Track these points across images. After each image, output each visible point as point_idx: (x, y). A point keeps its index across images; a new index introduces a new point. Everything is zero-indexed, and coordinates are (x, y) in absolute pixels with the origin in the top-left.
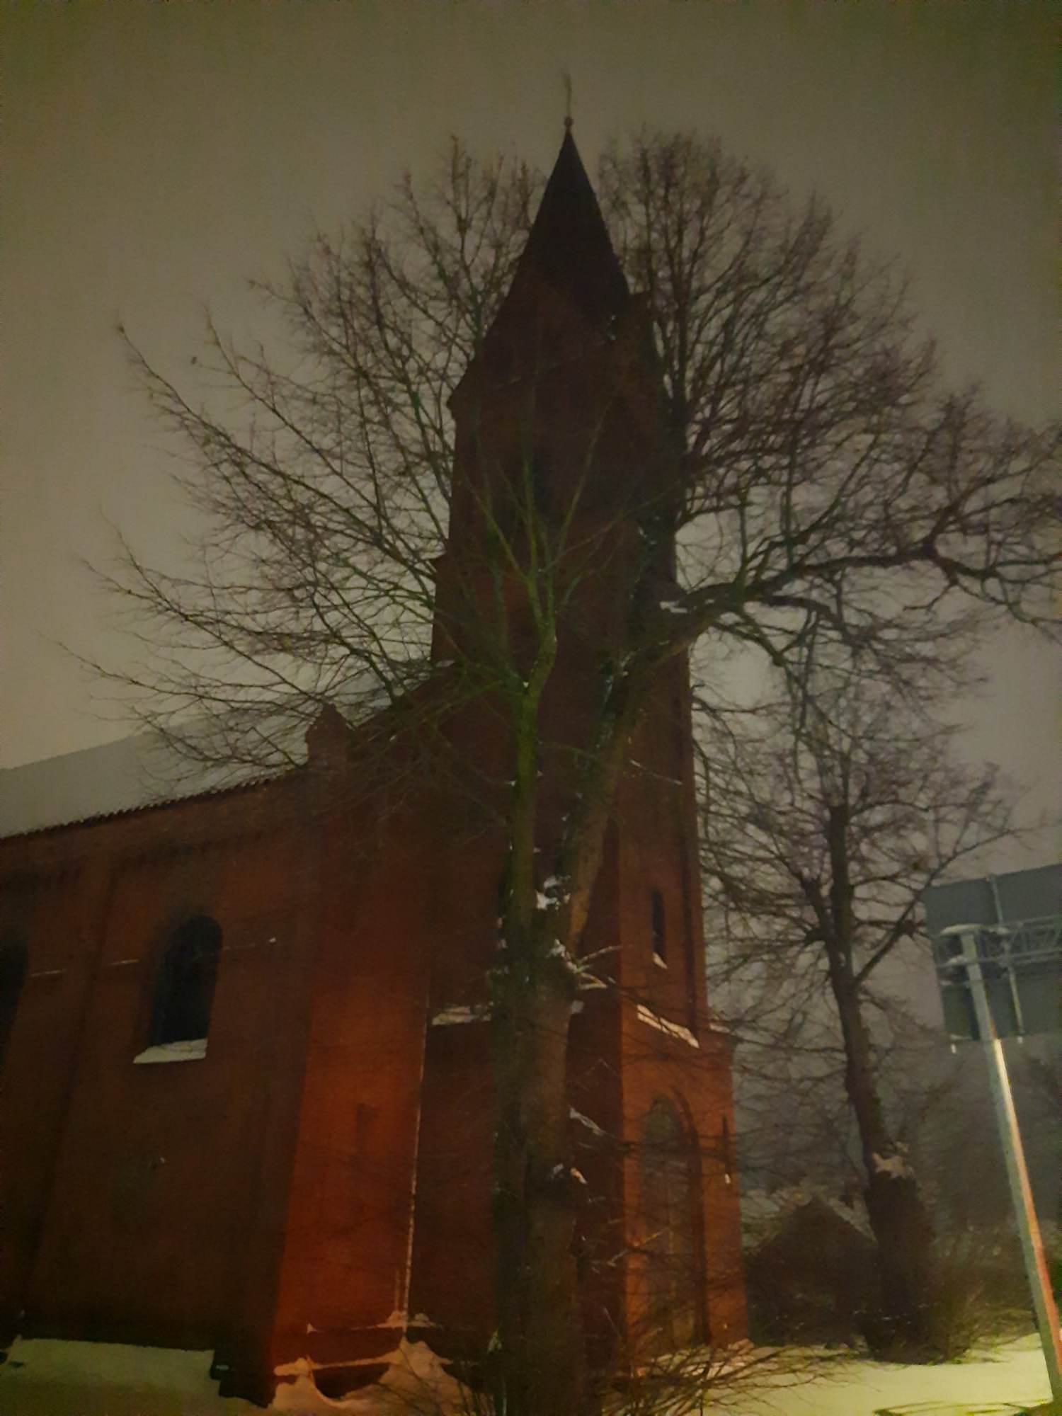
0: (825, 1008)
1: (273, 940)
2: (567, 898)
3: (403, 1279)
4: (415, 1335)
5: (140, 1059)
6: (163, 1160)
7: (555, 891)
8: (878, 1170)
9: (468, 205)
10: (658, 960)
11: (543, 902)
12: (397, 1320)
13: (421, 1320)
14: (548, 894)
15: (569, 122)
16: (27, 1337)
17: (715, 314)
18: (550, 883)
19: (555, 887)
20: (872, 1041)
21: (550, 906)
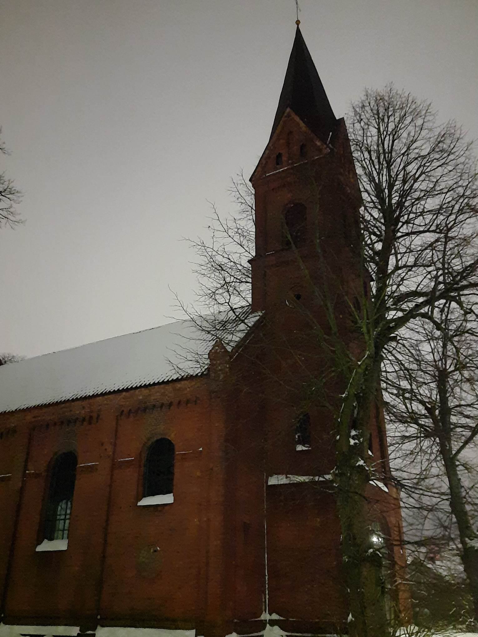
0: (438, 468)
1: (201, 449)
2: (361, 440)
3: (265, 598)
4: (273, 623)
5: (140, 503)
6: (158, 548)
7: (356, 437)
8: (469, 546)
9: (366, 163)
10: (370, 453)
11: (352, 442)
12: (265, 616)
13: (275, 617)
14: (353, 438)
15: (298, 22)
16: (103, 626)
17: (452, 190)
18: (353, 433)
19: (356, 435)
20: (462, 484)
21: (355, 444)
